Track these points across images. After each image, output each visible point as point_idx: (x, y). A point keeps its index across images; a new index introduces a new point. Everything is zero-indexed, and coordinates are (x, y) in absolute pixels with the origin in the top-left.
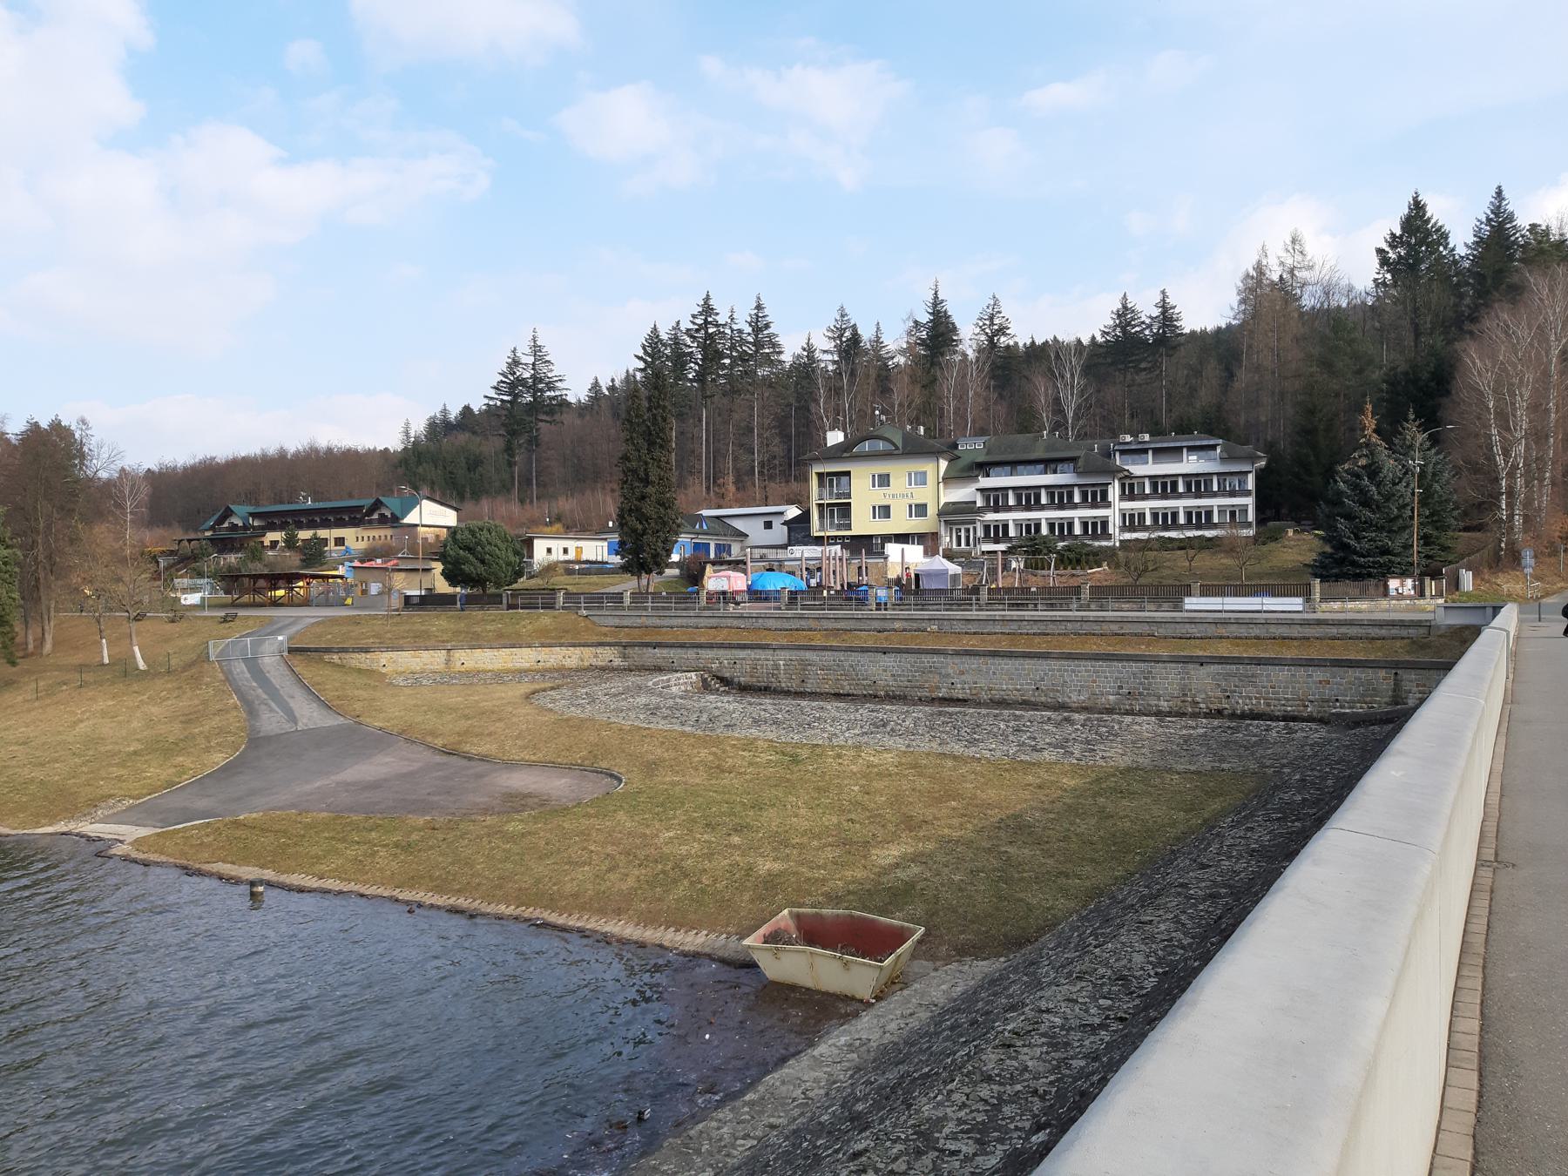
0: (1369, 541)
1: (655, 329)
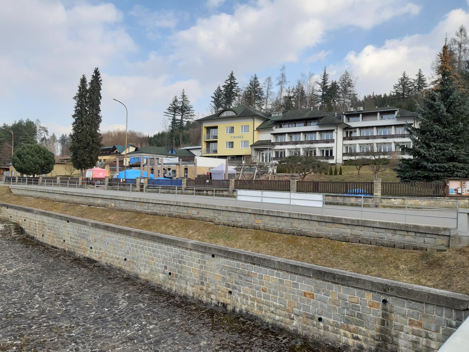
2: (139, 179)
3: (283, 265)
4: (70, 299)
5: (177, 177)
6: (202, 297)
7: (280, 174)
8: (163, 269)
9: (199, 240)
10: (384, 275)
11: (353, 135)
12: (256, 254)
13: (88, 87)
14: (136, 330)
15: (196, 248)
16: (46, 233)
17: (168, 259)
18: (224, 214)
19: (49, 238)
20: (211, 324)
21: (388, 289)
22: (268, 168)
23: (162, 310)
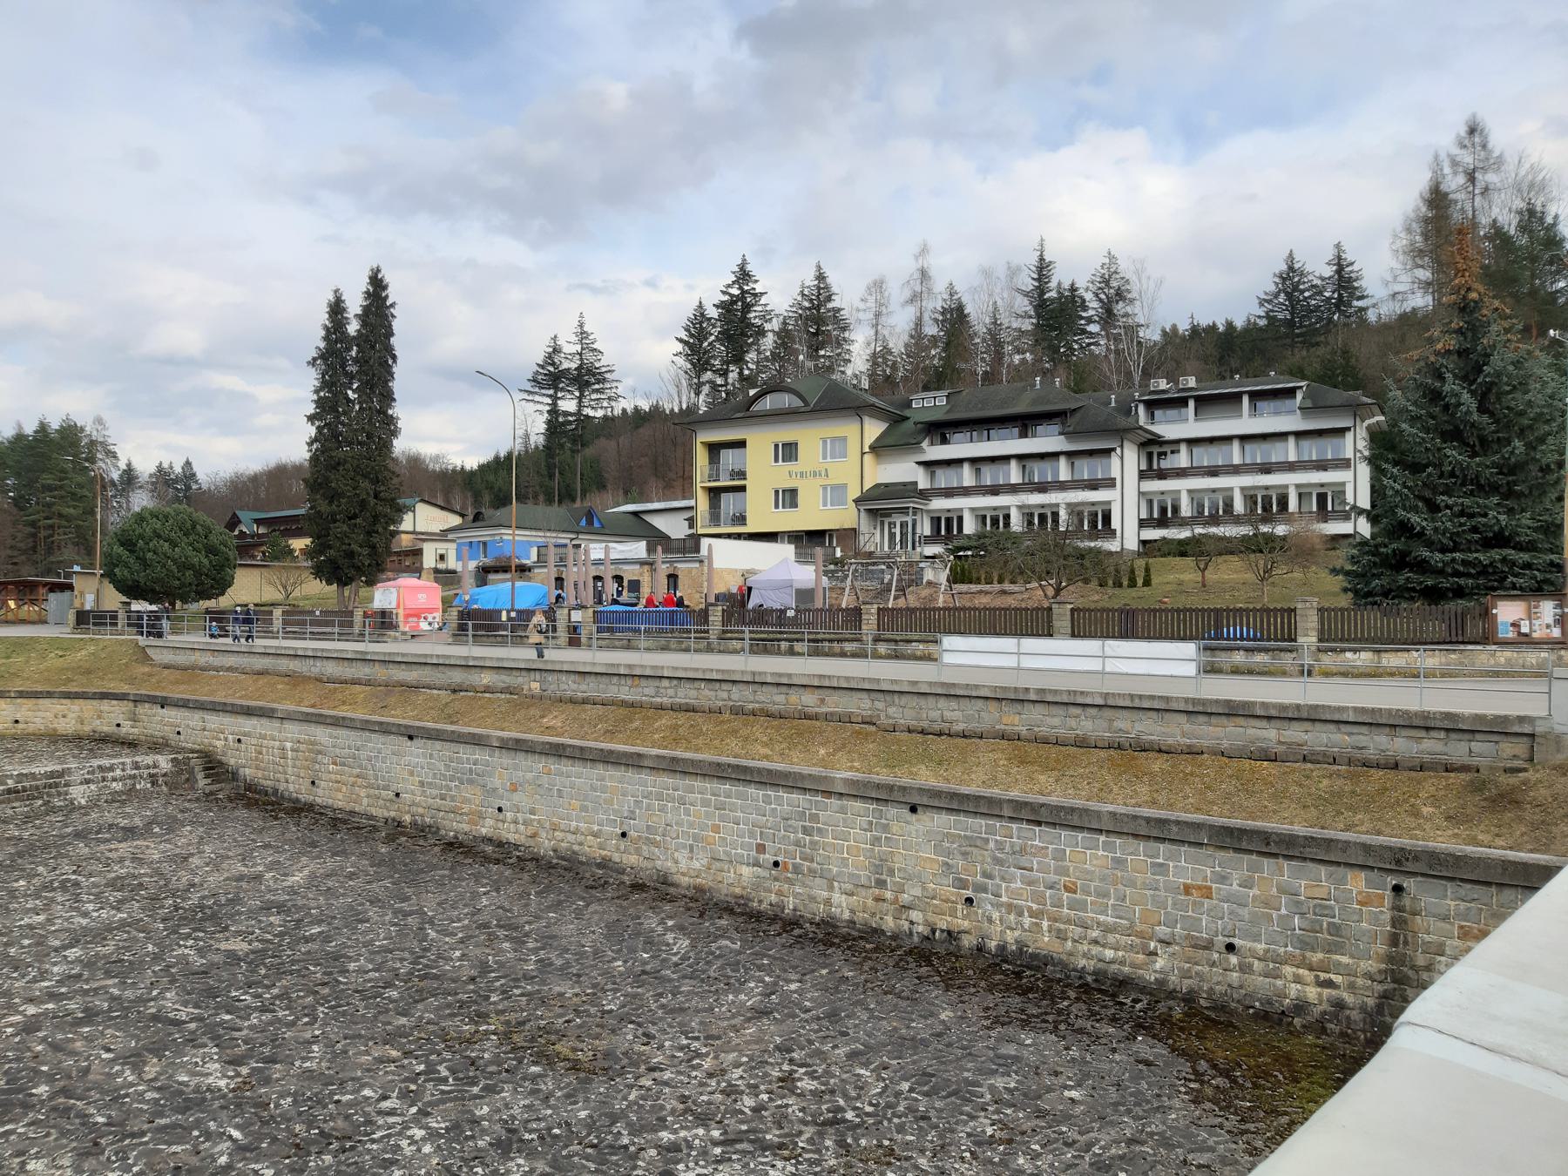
0: (1454, 515)
1: (700, 306)
3: (1126, 819)
7: (964, 587)
8: (754, 853)
9: (858, 770)
10: (1388, 831)
11: (1166, 464)
12: (1042, 799)
13: (353, 328)
15: (861, 792)
18: (902, 703)
21: (1407, 860)
22: (922, 569)
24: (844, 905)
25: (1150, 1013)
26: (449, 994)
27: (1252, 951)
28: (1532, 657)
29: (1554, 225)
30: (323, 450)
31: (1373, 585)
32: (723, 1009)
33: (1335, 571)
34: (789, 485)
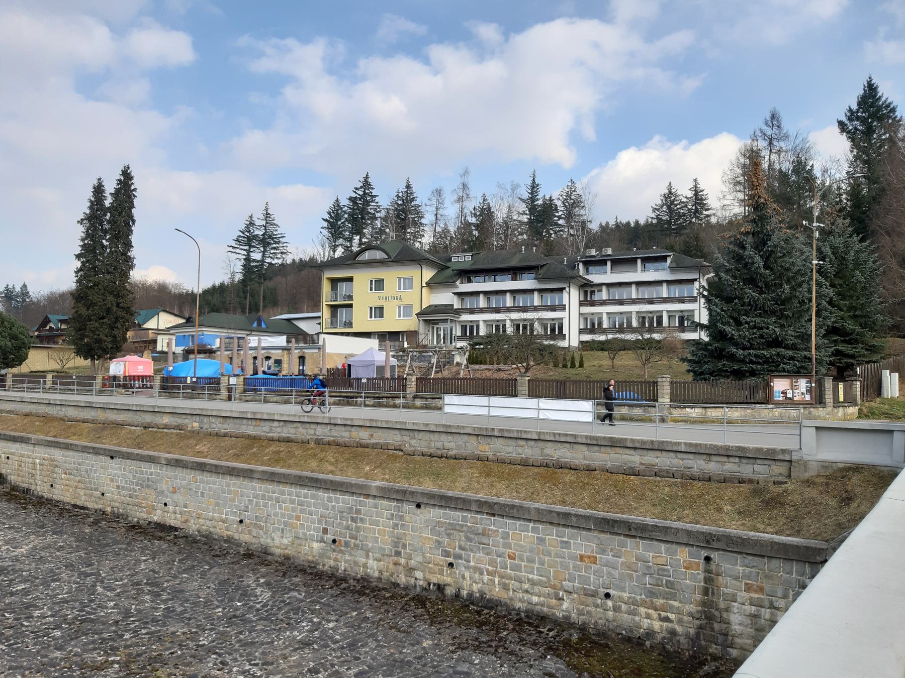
0: (750, 328)
2: (226, 378)
3: (545, 513)
4: (163, 590)
5: (284, 373)
6: (398, 576)
7: (477, 367)
8: (320, 534)
9: (387, 480)
10: (703, 521)
11: (596, 297)
12: (496, 500)
13: (108, 202)
14: (307, 631)
15: (386, 494)
16: (58, 481)
17: (331, 516)
18: (420, 438)
19: (68, 491)
20: (427, 617)
22: (453, 355)
23: (336, 600)
24: (375, 568)
25: (557, 639)
26: (97, 634)
27: (621, 599)
28: (793, 413)
29: (811, 170)
30: (84, 277)
31: (704, 368)
32: (281, 642)
33: (683, 360)
34: (379, 304)
